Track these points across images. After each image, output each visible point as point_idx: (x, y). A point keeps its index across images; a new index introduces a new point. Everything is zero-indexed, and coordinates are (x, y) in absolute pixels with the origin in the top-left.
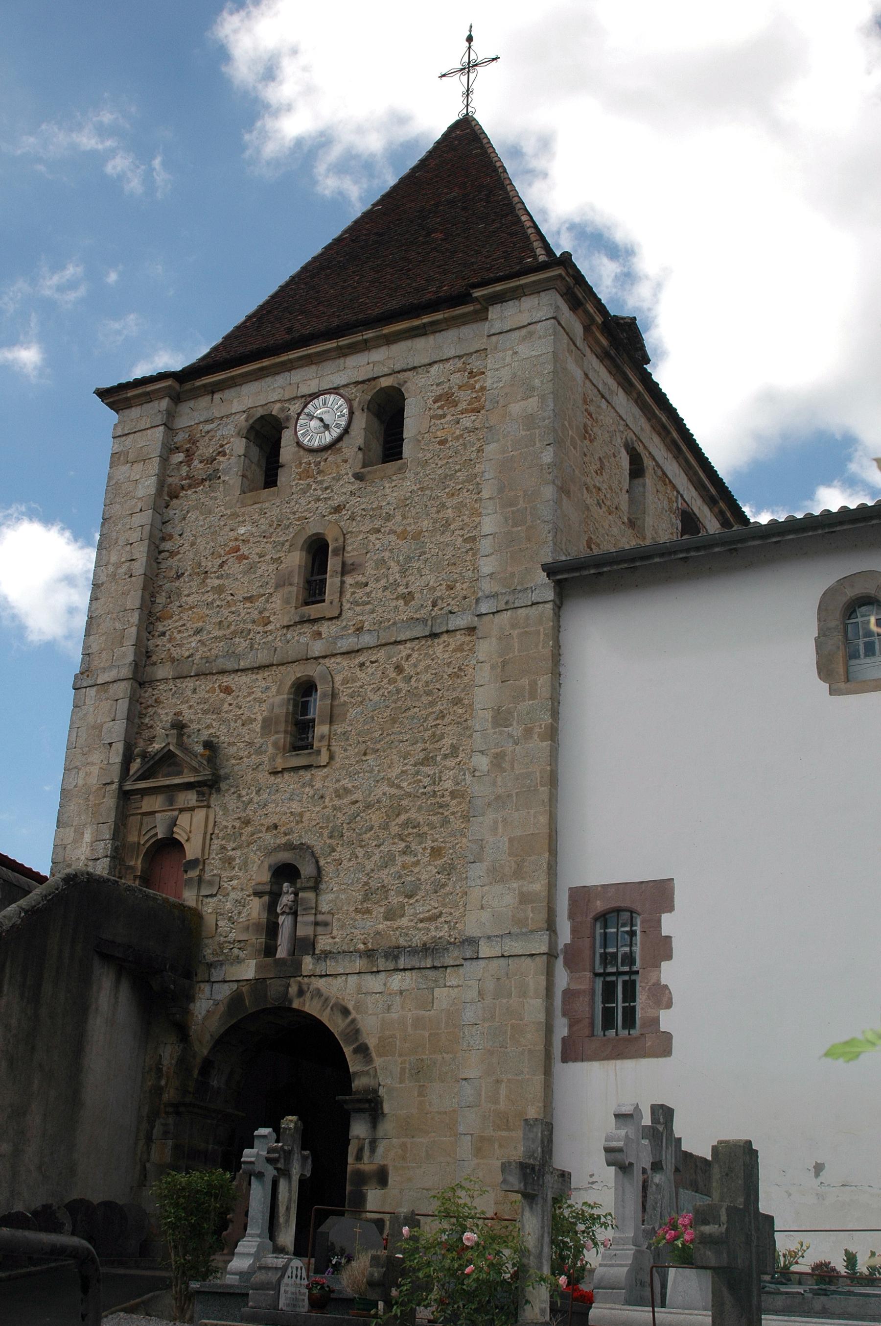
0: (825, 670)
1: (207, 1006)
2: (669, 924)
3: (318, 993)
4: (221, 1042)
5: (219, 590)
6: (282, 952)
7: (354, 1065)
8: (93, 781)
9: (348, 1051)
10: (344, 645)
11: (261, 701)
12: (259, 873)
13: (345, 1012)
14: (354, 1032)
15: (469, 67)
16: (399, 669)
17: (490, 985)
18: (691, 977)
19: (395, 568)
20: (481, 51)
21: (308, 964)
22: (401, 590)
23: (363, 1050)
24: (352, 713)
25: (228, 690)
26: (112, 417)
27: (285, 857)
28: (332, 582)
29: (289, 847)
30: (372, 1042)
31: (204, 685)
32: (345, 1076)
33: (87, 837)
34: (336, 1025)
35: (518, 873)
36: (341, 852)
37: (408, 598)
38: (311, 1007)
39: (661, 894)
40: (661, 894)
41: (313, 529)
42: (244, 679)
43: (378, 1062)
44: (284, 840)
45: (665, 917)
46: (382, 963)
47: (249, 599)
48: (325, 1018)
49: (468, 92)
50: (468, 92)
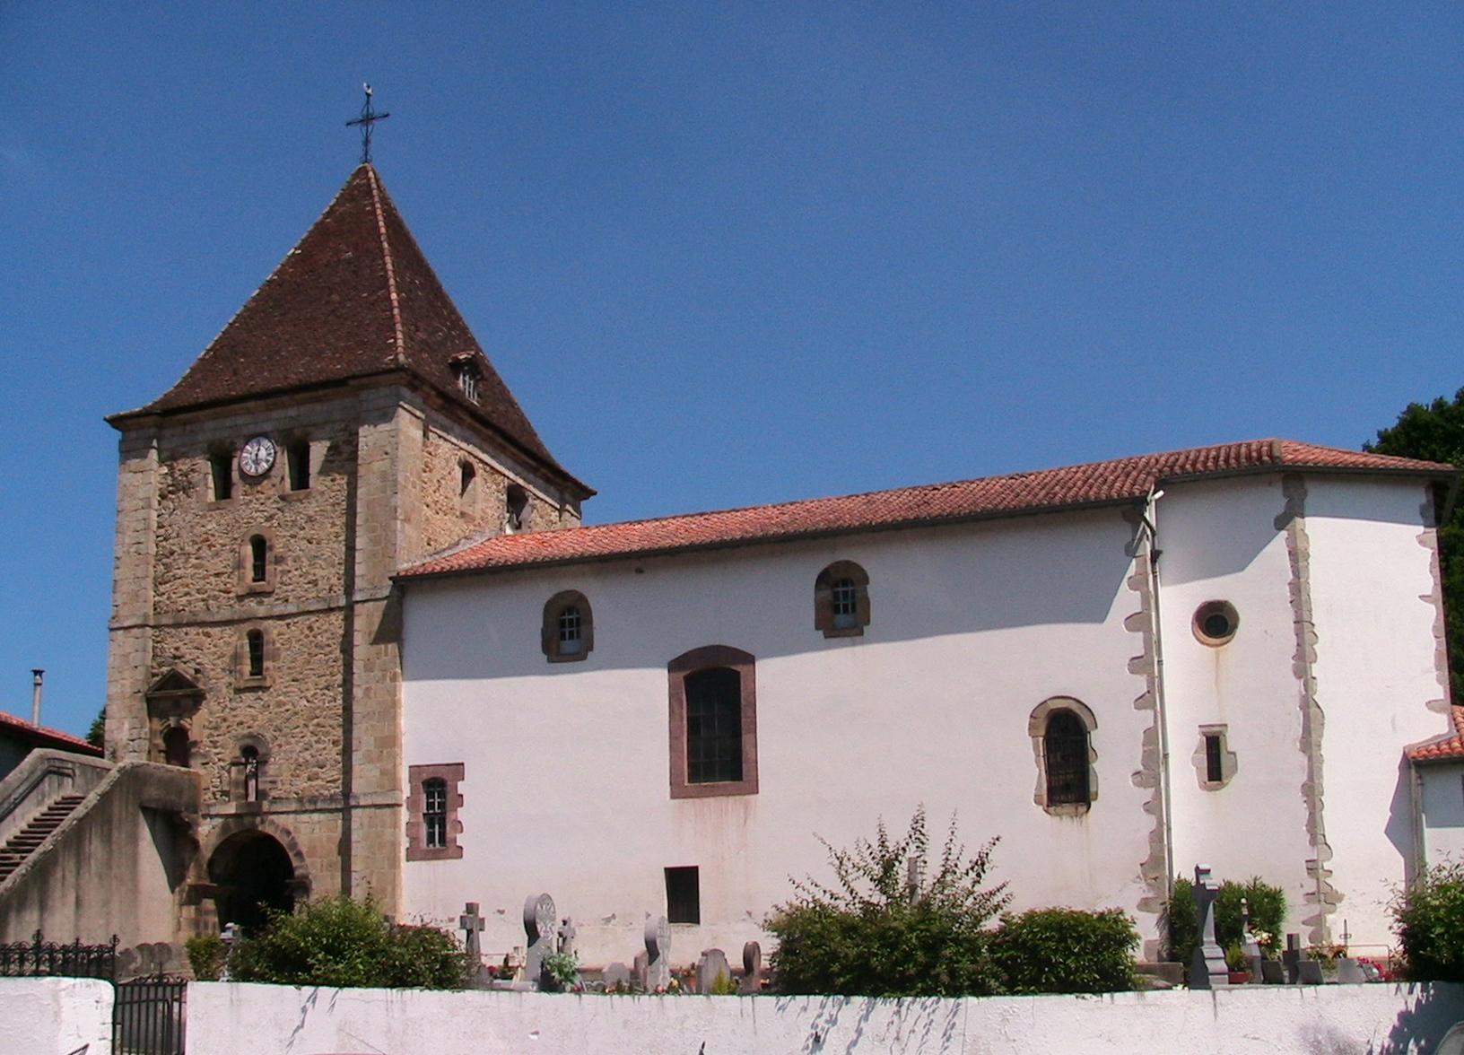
0: (546, 648)
1: (207, 832)
2: (462, 787)
3: (272, 822)
4: (218, 850)
5: (195, 567)
6: (252, 798)
7: (295, 863)
8: (128, 691)
9: (291, 855)
10: (278, 610)
11: (228, 644)
12: (232, 751)
13: (289, 833)
14: (294, 845)
15: (367, 120)
16: (310, 628)
17: (366, 821)
18: (474, 813)
19: (306, 563)
20: (377, 109)
21: (266, 806)
22: (311, 577)
23: (299, 854)
24: (283, 655)
25: (208, 635)
26: (117, 435)
27: (249, 741)
28: (269, 568)
29: (251, 736)
30: (304, 850)
31: (193, 631)
32: (289, 870)
33: (127, 726)
34: (284, 840)
35: (380, 759)
36: (281, 740)
37: (315, 583)
38: (269, 830)
39: (458, 769)
40: (458, 769)
41: (255, 532)
42: (217, 630)
43: (308, 861)
44: (246, 731)
45: (460, 784)
46: (308, 806)
47: (217, 575)
48: (277, 836)
49: (367, 142)
50: (367, 142)
